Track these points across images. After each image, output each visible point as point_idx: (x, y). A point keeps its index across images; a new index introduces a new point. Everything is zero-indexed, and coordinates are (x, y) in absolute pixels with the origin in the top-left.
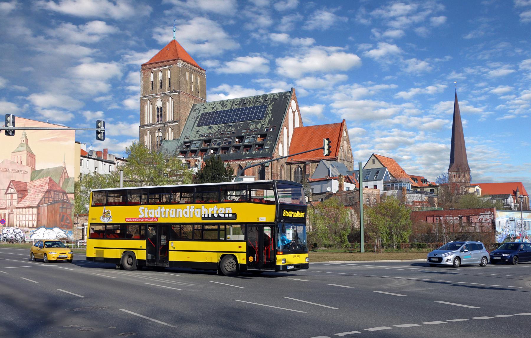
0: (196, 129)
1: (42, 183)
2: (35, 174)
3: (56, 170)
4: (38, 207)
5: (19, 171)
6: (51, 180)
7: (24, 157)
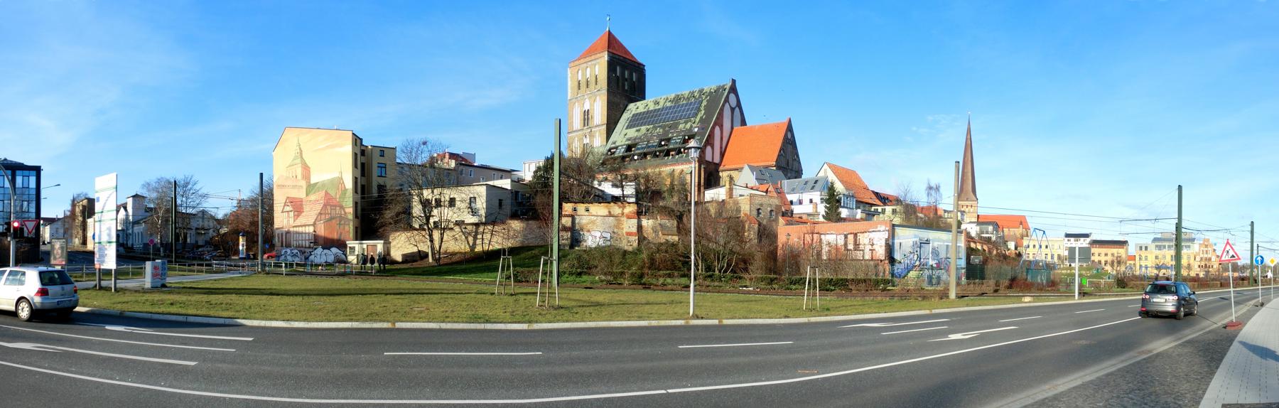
0: (625, 131)
1: (317, 196)
2: (311, 188)
3: (332, 181)
4: (314, 225)
5: (294, 187)
6: (327, 194)
7: (299, 171)
